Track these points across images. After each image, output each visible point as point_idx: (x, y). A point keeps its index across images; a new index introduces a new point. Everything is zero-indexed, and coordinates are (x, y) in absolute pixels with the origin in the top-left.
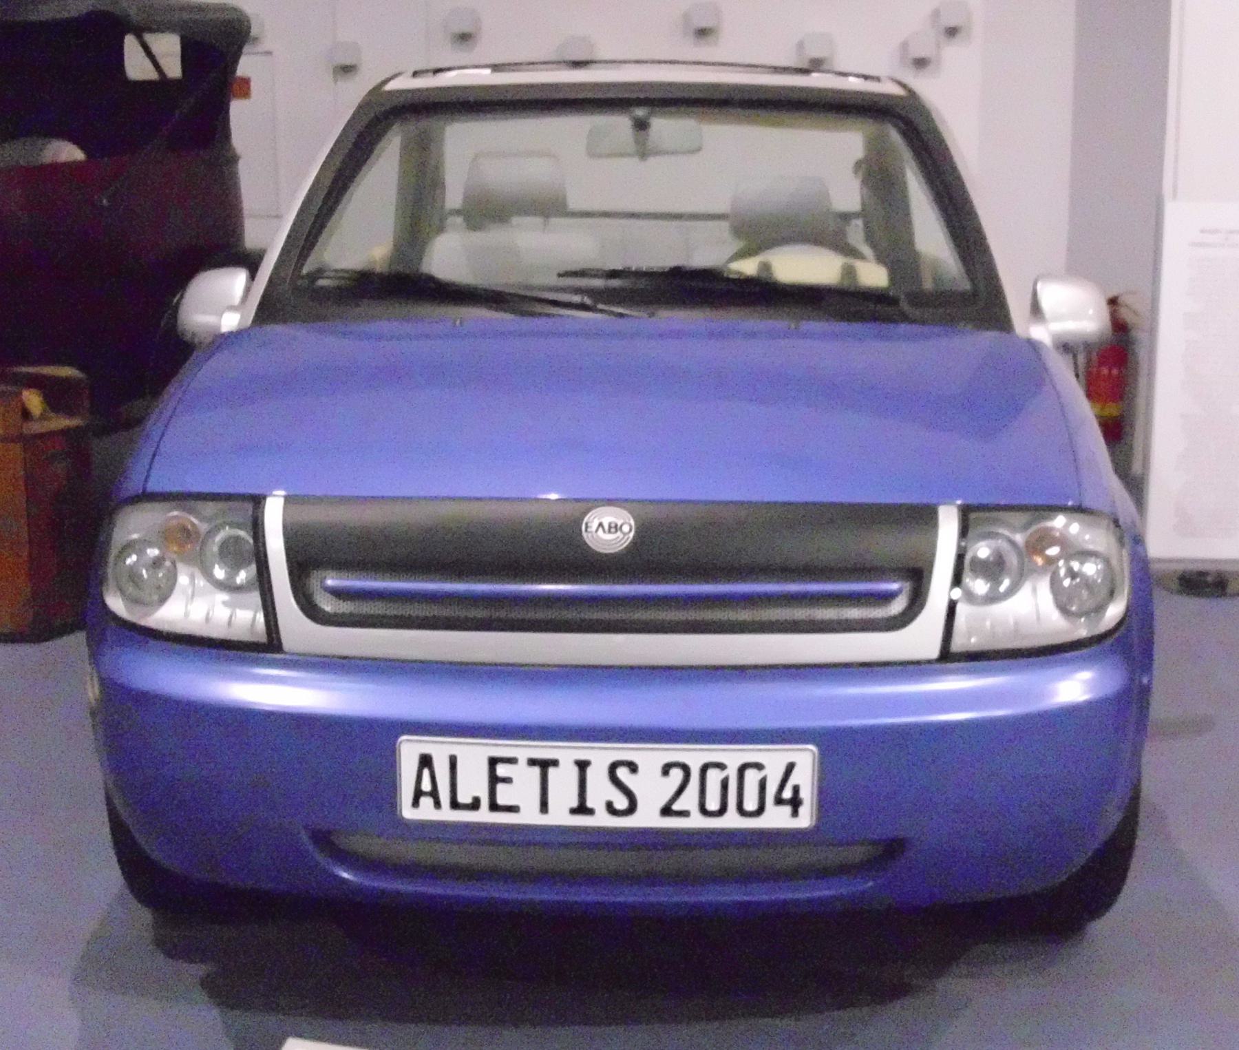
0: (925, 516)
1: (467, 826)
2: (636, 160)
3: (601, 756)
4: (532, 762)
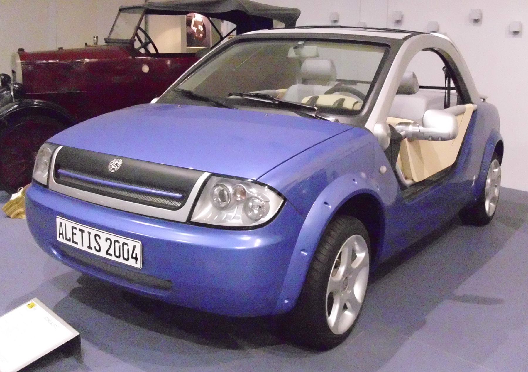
0: (58, 145)
1: (67, 245)
2: (106, 37)
3: (94, 232)
4: (80, 230)
